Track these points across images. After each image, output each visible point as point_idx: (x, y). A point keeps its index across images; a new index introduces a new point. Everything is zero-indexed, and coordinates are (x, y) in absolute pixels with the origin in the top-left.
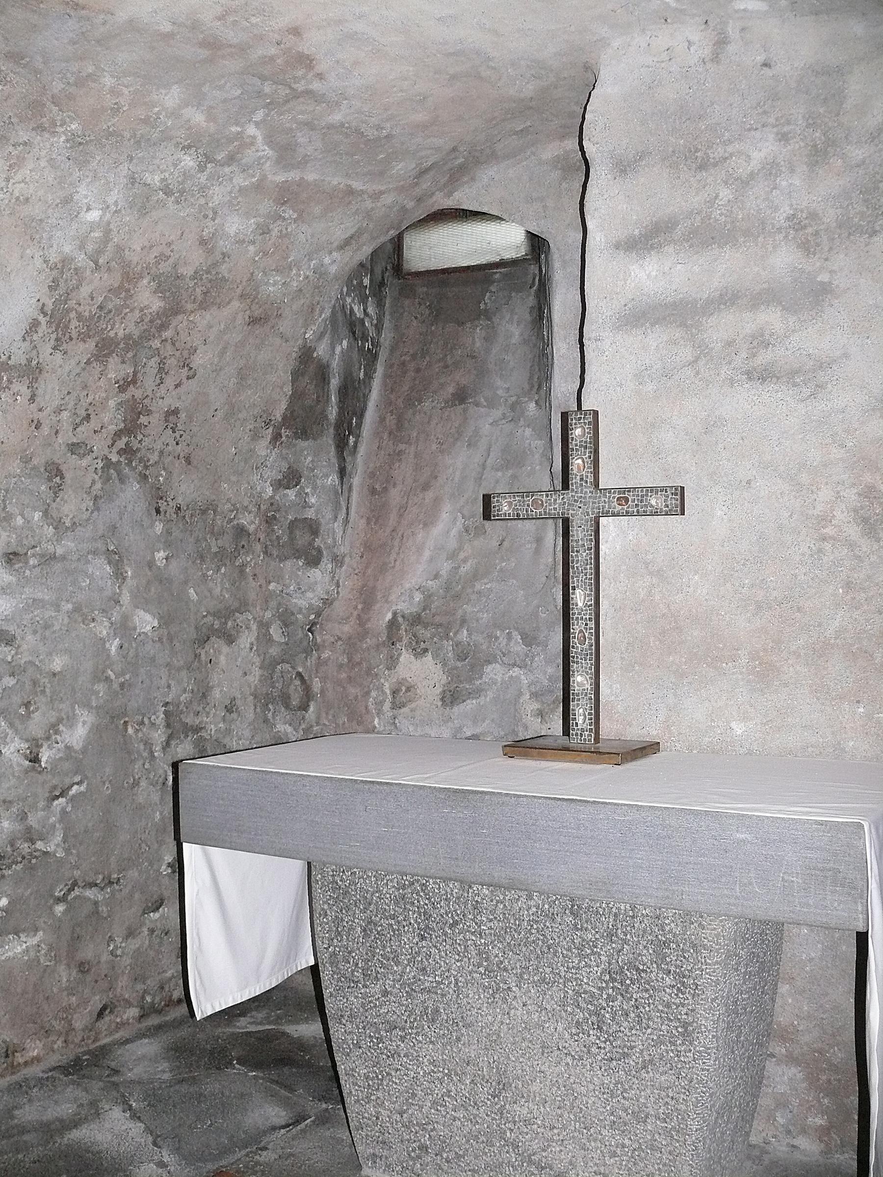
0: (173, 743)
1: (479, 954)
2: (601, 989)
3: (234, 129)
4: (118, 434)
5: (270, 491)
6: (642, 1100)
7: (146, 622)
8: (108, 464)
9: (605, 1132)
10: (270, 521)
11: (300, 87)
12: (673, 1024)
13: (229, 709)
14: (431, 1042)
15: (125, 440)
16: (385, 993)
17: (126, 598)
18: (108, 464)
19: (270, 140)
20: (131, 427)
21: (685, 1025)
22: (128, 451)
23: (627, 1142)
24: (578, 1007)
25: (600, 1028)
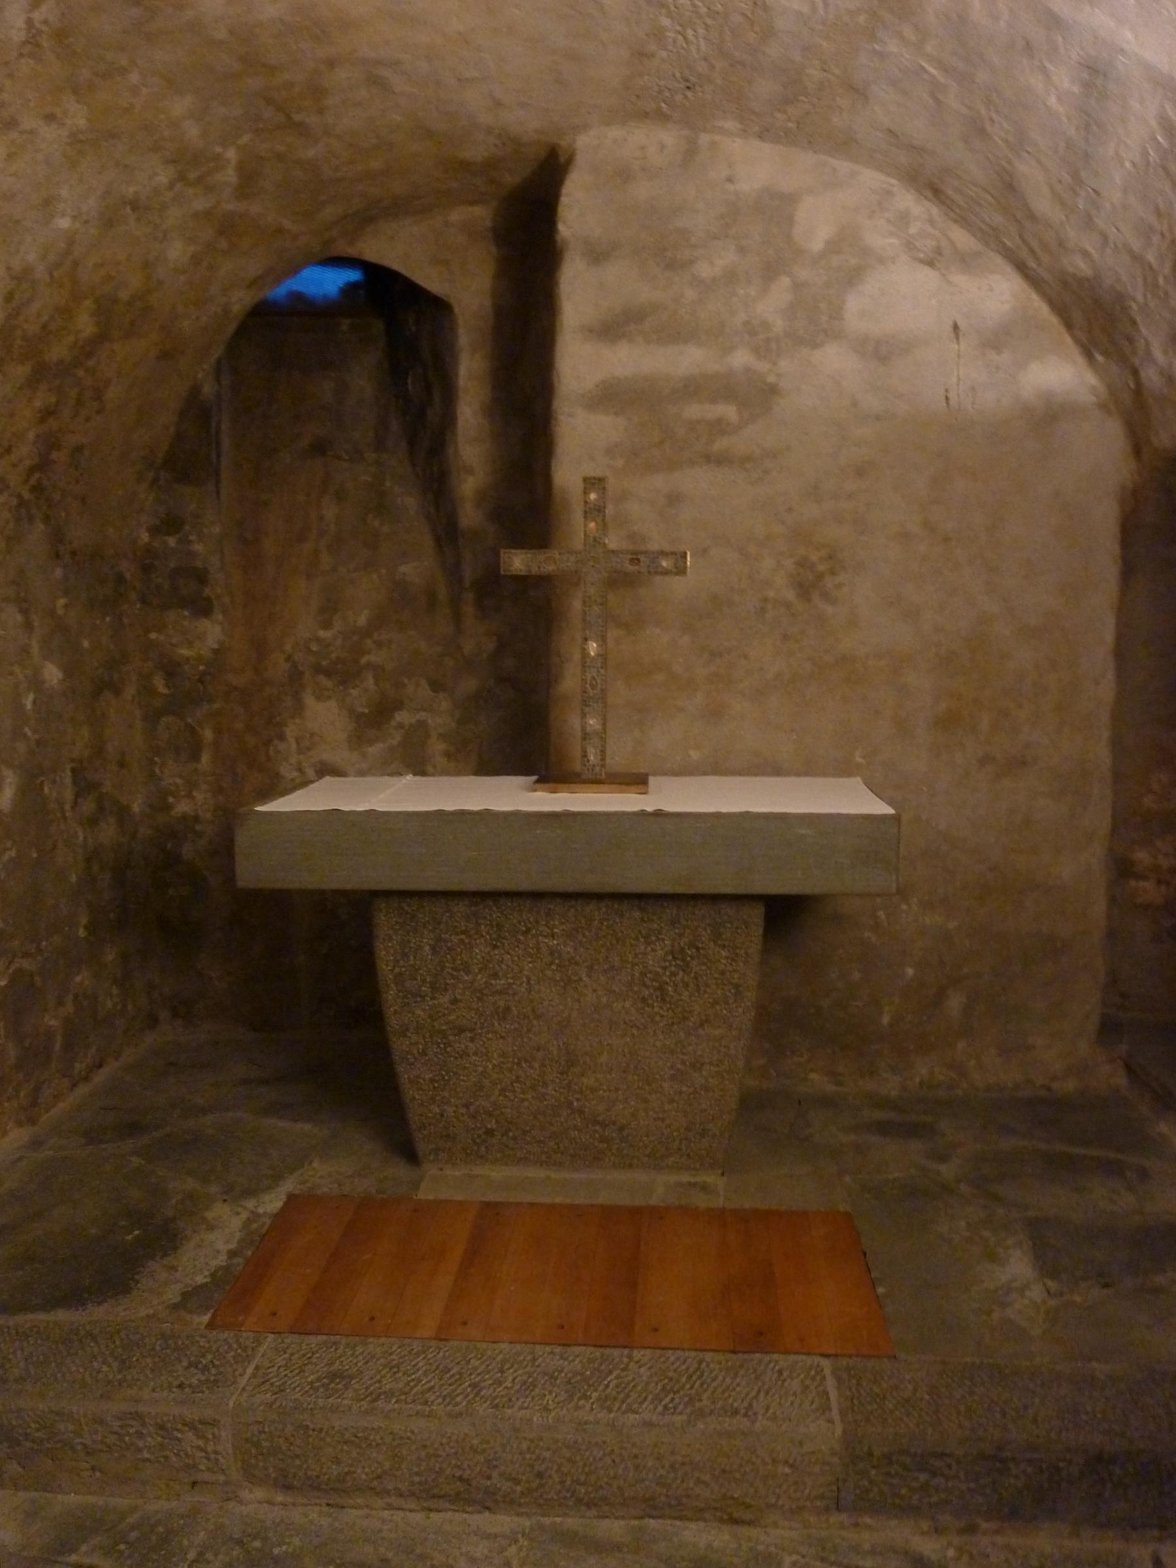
0: (80, 800)
1: (552, 953)
2: (665, 968)
3: (218, 149)
4: (32, 470)
5: (145, 537)
6: (699, 1053)
7: (53, 674)
8: (22, 502)
9: (665, 1085)
10: (147, 569)
11: (297, 118)
12: (726, 988)
13: (122, 765)
14: (502, 1037)
15: (37, 475)
16: (455, 1001)
17: (35, 649)
18: (22, 502)
19: (241, 168)
20: (43, 464)
21: (737, 986)
22: (38, 489)
23: (684, 1089)
24: (645, 985)
25: (663, 1000)
